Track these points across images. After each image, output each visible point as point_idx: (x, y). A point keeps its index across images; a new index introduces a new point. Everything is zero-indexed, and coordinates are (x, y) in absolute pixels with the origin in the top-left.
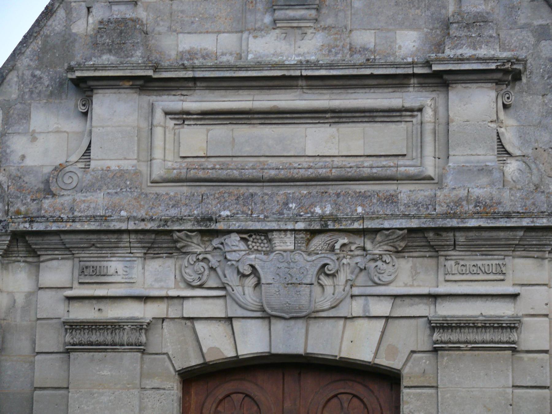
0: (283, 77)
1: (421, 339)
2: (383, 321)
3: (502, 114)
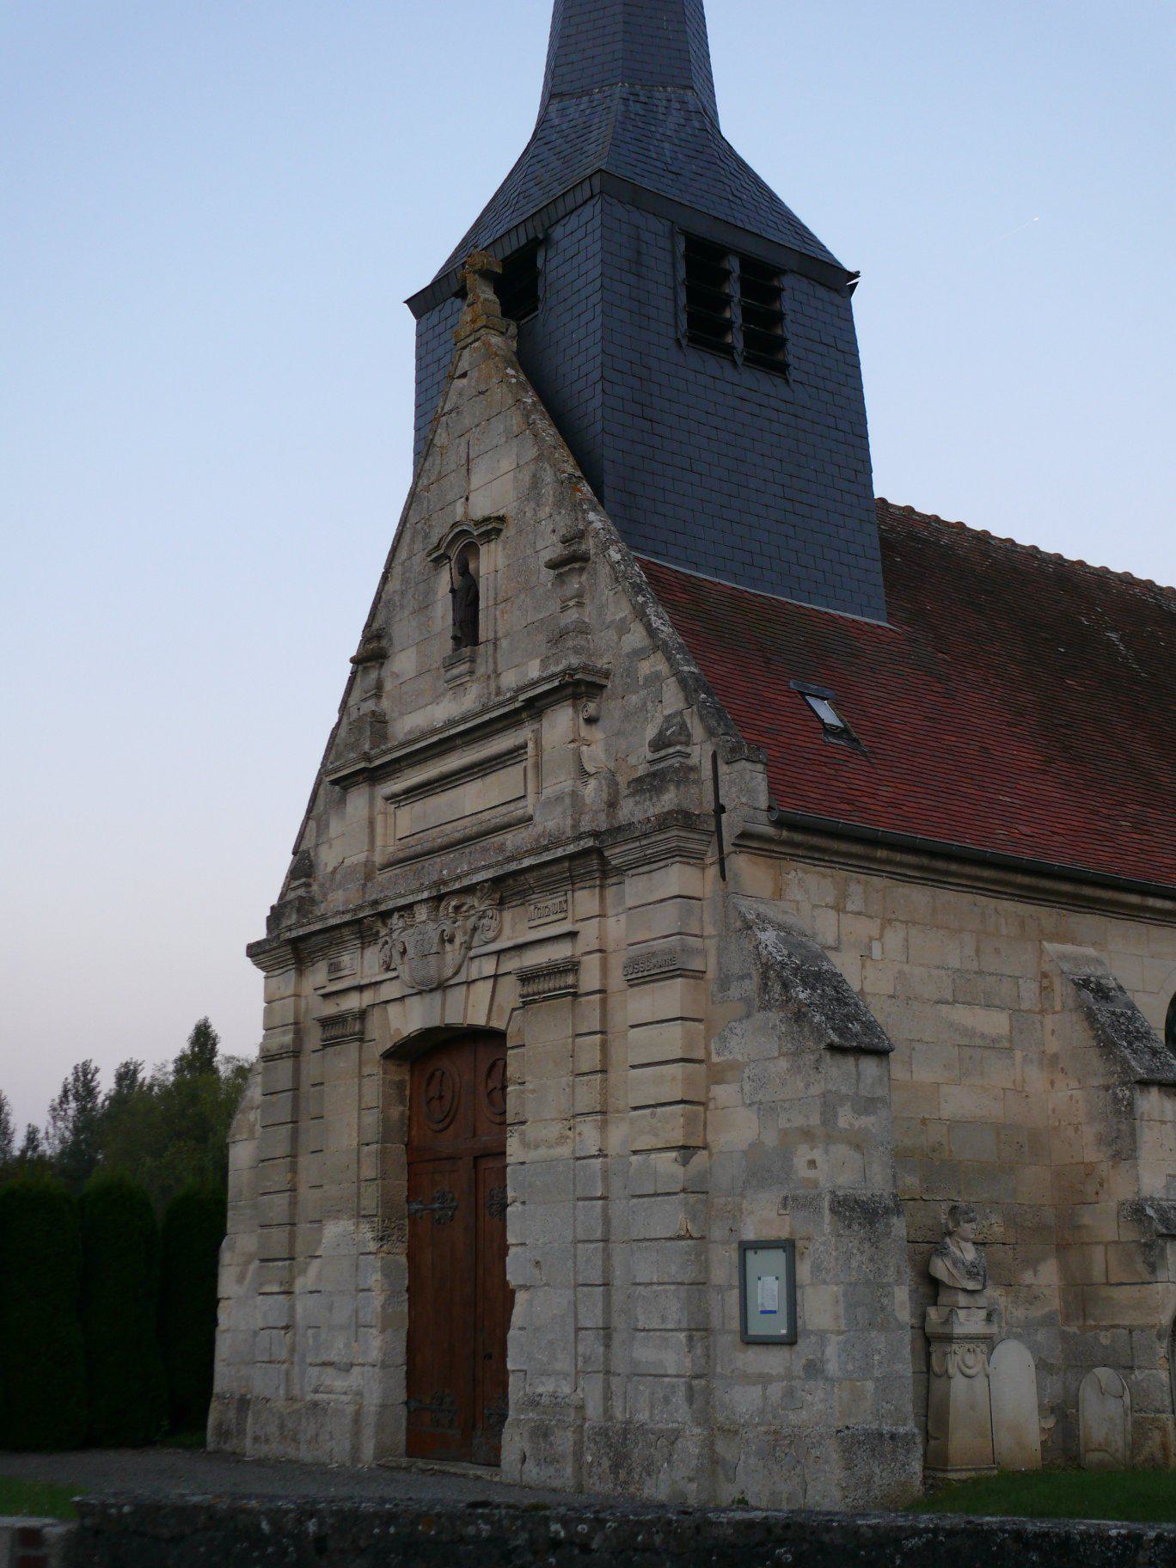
0: (441, 742)
1: (510, 992)
2: (491, 981)
3: (584, 731)
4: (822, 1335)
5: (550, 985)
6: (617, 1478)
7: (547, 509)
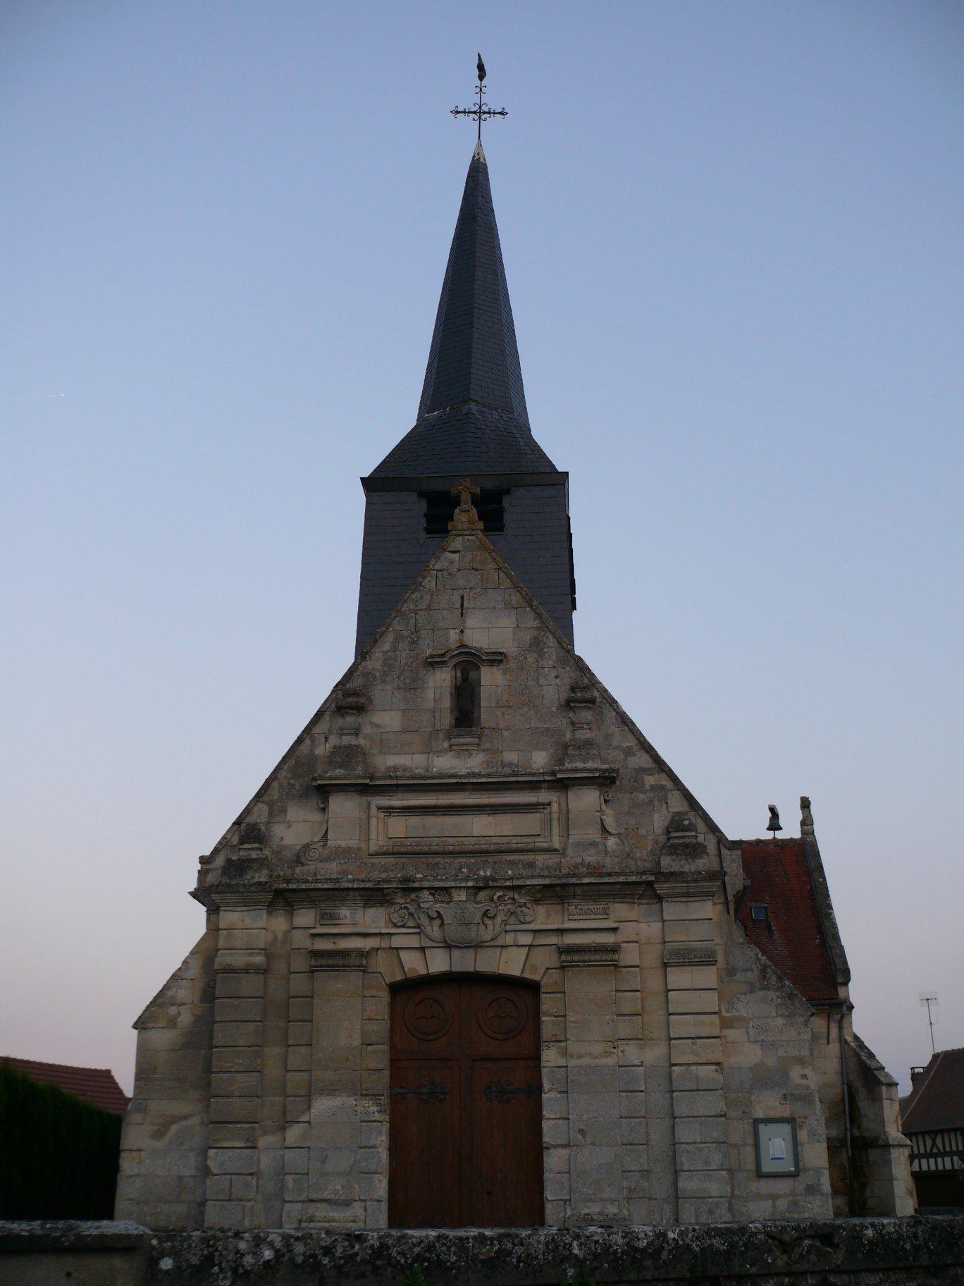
1: (554, 961)
4: (818, 1170)
5: (572, 958)
6: (297, 1239)
7: (550, 662)
